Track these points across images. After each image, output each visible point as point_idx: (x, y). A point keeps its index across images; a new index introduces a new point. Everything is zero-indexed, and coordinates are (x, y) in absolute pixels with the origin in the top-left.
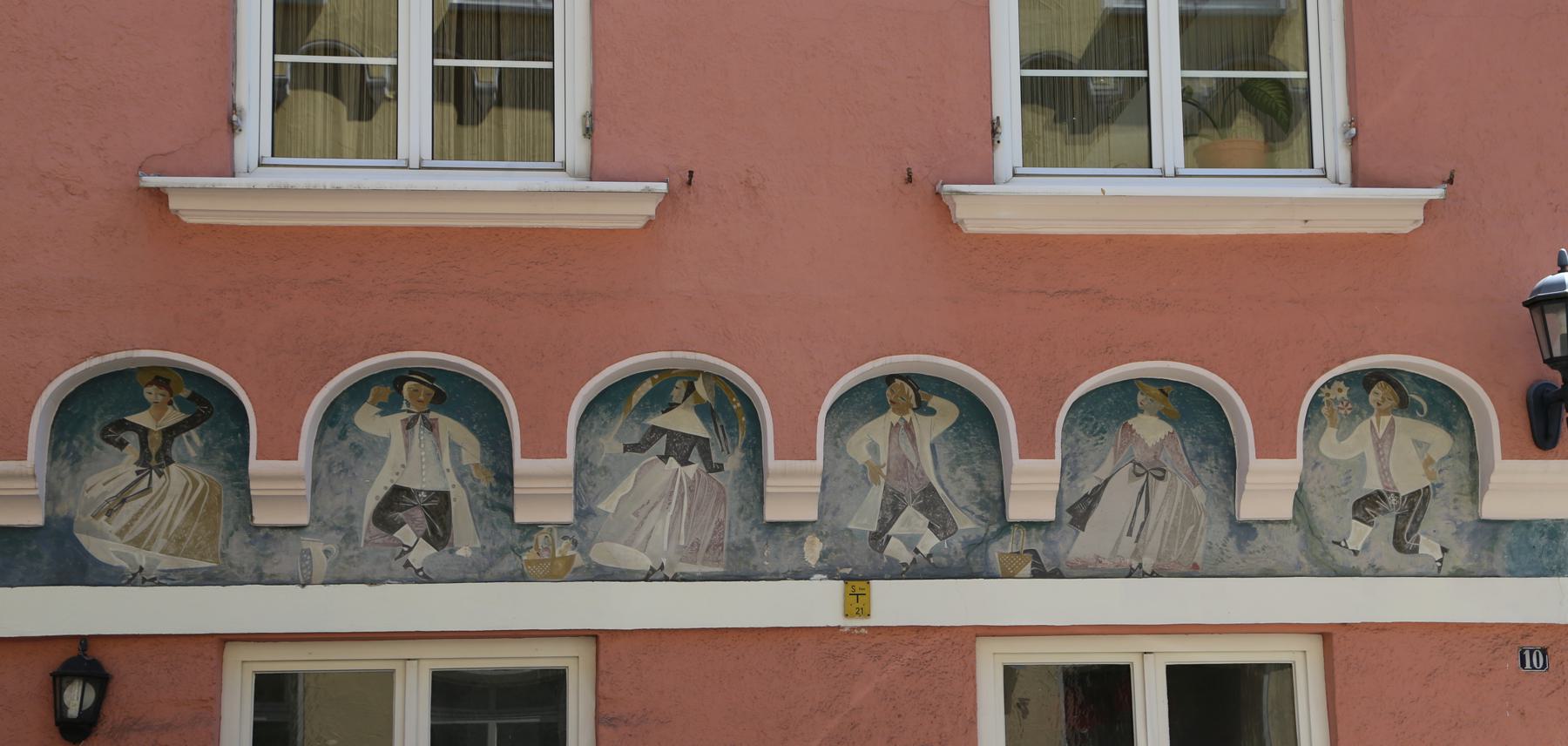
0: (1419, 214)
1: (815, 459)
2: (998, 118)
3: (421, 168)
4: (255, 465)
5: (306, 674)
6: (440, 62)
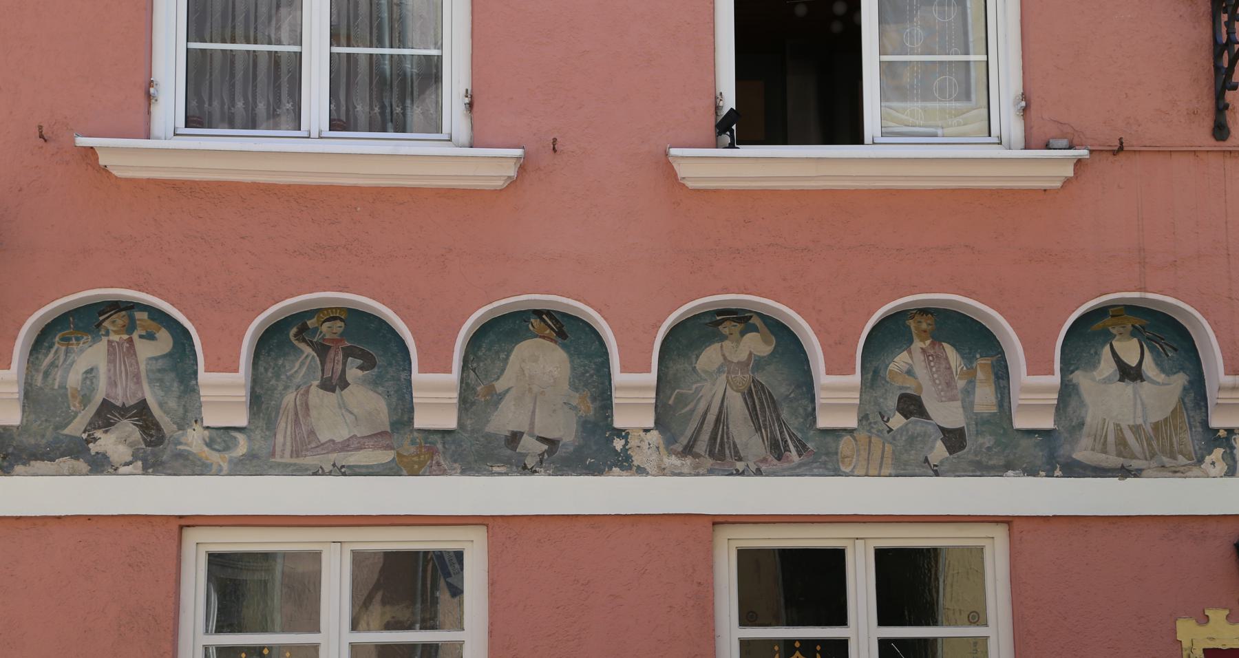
0: (1069, 172)
1: (450, 372)
2: (721, 94)
3: (320, 137)
4: (203, 376)
5: (948, 548)
6: (336, 50)
